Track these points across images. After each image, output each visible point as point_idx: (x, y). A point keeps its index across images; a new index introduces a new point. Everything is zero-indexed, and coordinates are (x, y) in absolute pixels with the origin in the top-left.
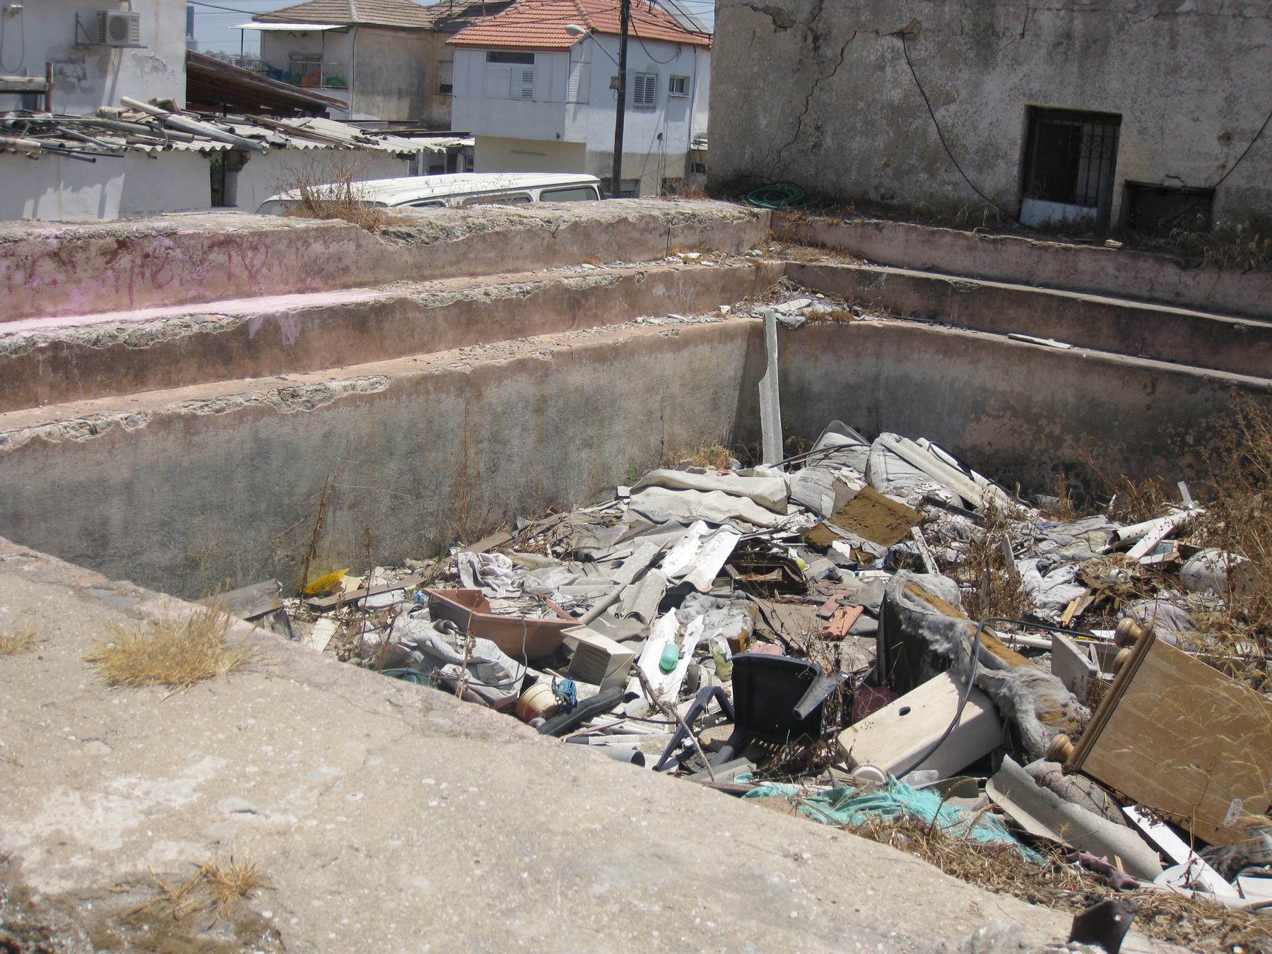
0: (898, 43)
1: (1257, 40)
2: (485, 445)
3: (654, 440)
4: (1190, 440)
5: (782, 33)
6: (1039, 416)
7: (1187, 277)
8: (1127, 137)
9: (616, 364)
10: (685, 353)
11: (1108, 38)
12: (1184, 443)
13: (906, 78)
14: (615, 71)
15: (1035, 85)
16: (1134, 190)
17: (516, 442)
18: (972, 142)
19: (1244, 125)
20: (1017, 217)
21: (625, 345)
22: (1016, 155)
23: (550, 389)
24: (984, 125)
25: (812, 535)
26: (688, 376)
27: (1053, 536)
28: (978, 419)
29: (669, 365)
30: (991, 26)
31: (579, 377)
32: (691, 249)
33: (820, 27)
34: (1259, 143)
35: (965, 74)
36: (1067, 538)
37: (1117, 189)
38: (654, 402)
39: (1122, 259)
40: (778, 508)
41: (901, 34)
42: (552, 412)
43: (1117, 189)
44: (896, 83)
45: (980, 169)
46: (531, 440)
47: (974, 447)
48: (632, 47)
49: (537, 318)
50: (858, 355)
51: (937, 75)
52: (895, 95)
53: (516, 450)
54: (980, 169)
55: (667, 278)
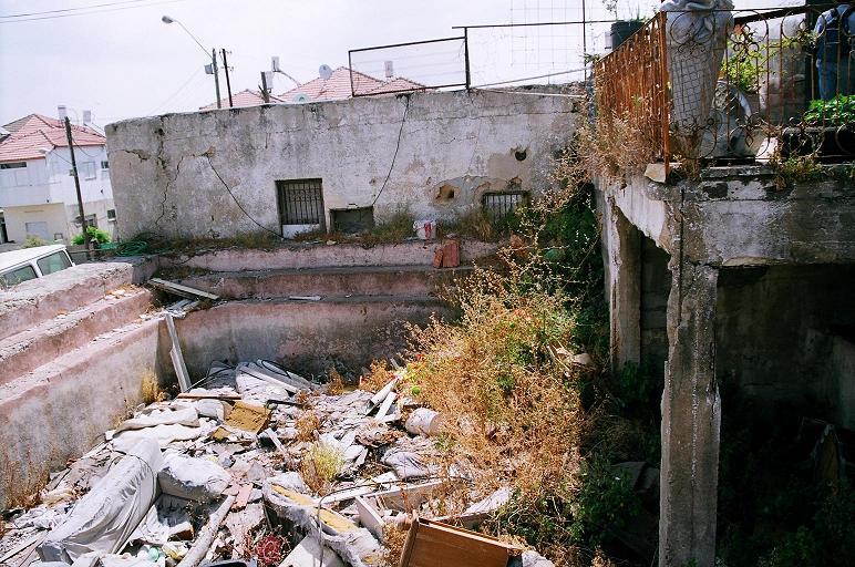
0: (206, 159)
1: (378, 135)
2: (18, 445)
3: (120, 401)
4: (388, 332)
5: (144, 162)
6: (315, 335)
7: (369, 252)
8: (326, 188)
9: (89, 371)
10: (126, 350)
11: (308, 143)
12: (386, 334)
13: (213, 176)
14: (72, 168)
15: (278, 171)
16: (334, 212)
17: (38, 435)
18: (252, 202)
19: (381, 174)
20: (282, 235)
21: (91, 359)
22: (275, 205)
23: (52, 397)
24: (256, 194)
25: (216, 435)
26: (131, 361)
27: (337, 408)
28: (285, 343)
29: (119, 359)
30: (250, 146)
31: (68, 386)
32: (118, 288)
33: (164, 156)
34: (389, 181)
35: (242, 170)
36: (345, 408)
37: (327, 214)
38: (115, 382)
39: (337, 249)
40: (194, 424)
41: (206, 154)
42: (56, 410)
43: (327, 214)
44: (208, 179)
45: (258, 214)
46: (47, 429)
47: (286, 356)
48: (76, 151)
49: (35, 358)
50: (218, 324)
51: (228, 172)
52: (210, 185)
53: (38, 440)
54: (258, 214)
55: (108, 311)
